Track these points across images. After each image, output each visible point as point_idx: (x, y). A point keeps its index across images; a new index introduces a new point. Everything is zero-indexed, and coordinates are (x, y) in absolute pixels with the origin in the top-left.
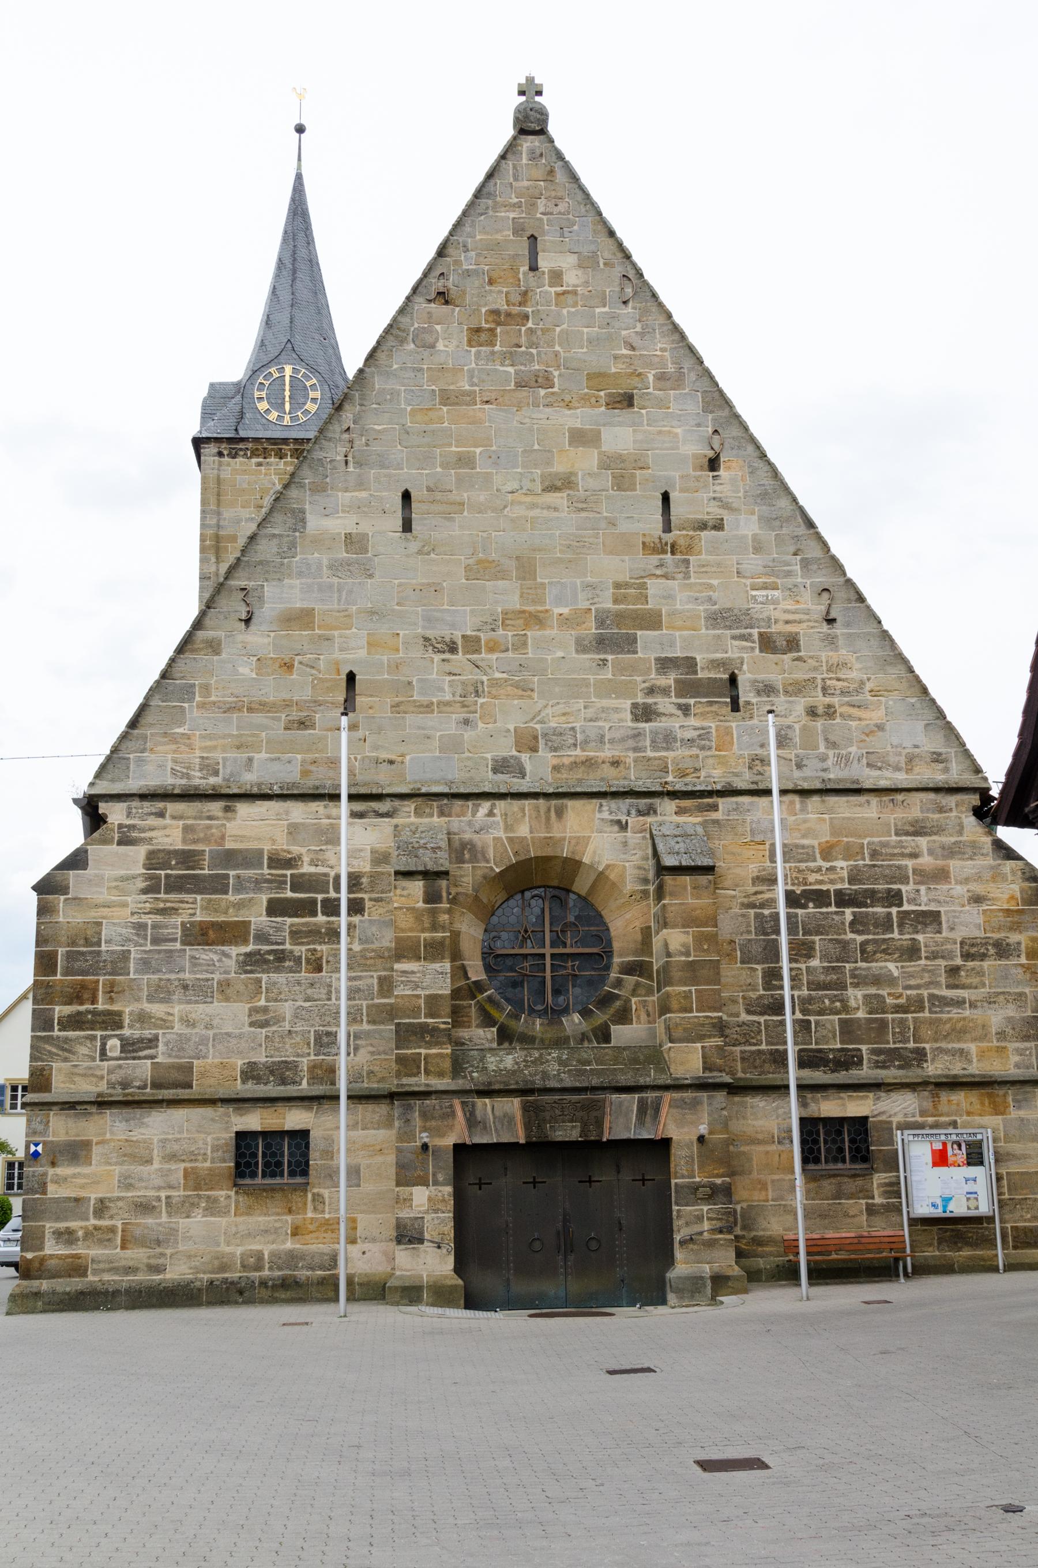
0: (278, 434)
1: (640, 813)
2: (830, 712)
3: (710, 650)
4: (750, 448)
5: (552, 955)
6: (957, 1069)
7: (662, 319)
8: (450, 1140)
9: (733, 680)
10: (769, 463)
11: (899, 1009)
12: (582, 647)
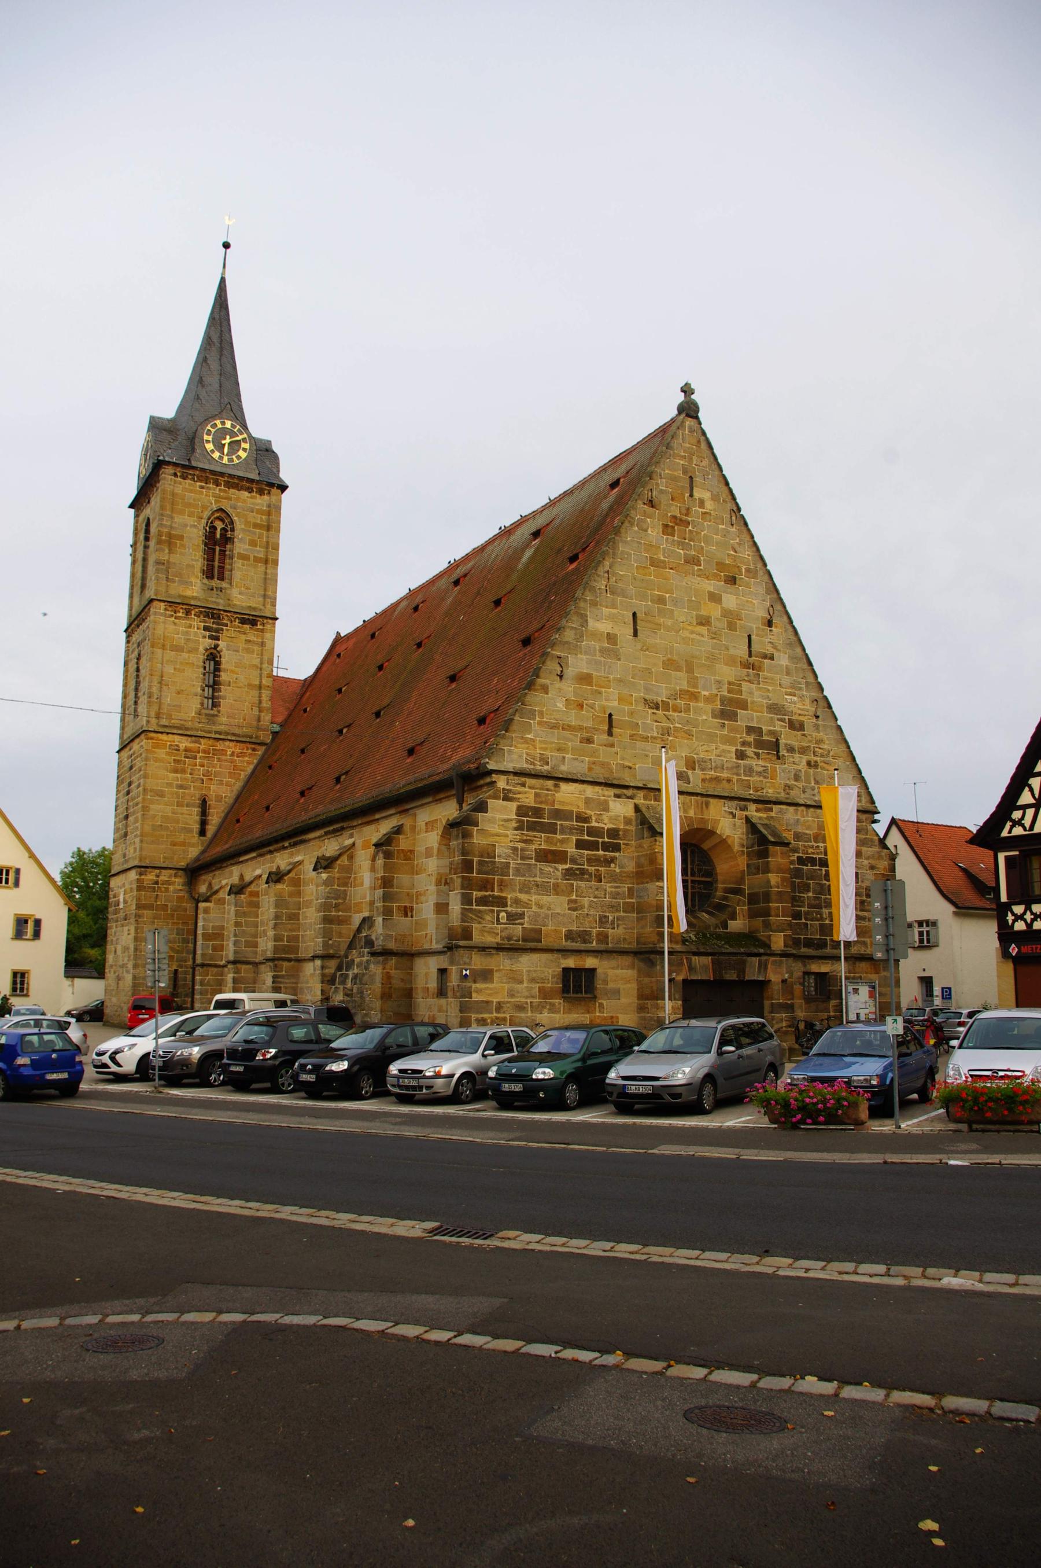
0: (218, 469)
1: (741, 810)
2: (816, 765)
4: (785, 618)
5: (692, 881)
7: (748, 538)
10: (794, 628)
12: (714, 716)
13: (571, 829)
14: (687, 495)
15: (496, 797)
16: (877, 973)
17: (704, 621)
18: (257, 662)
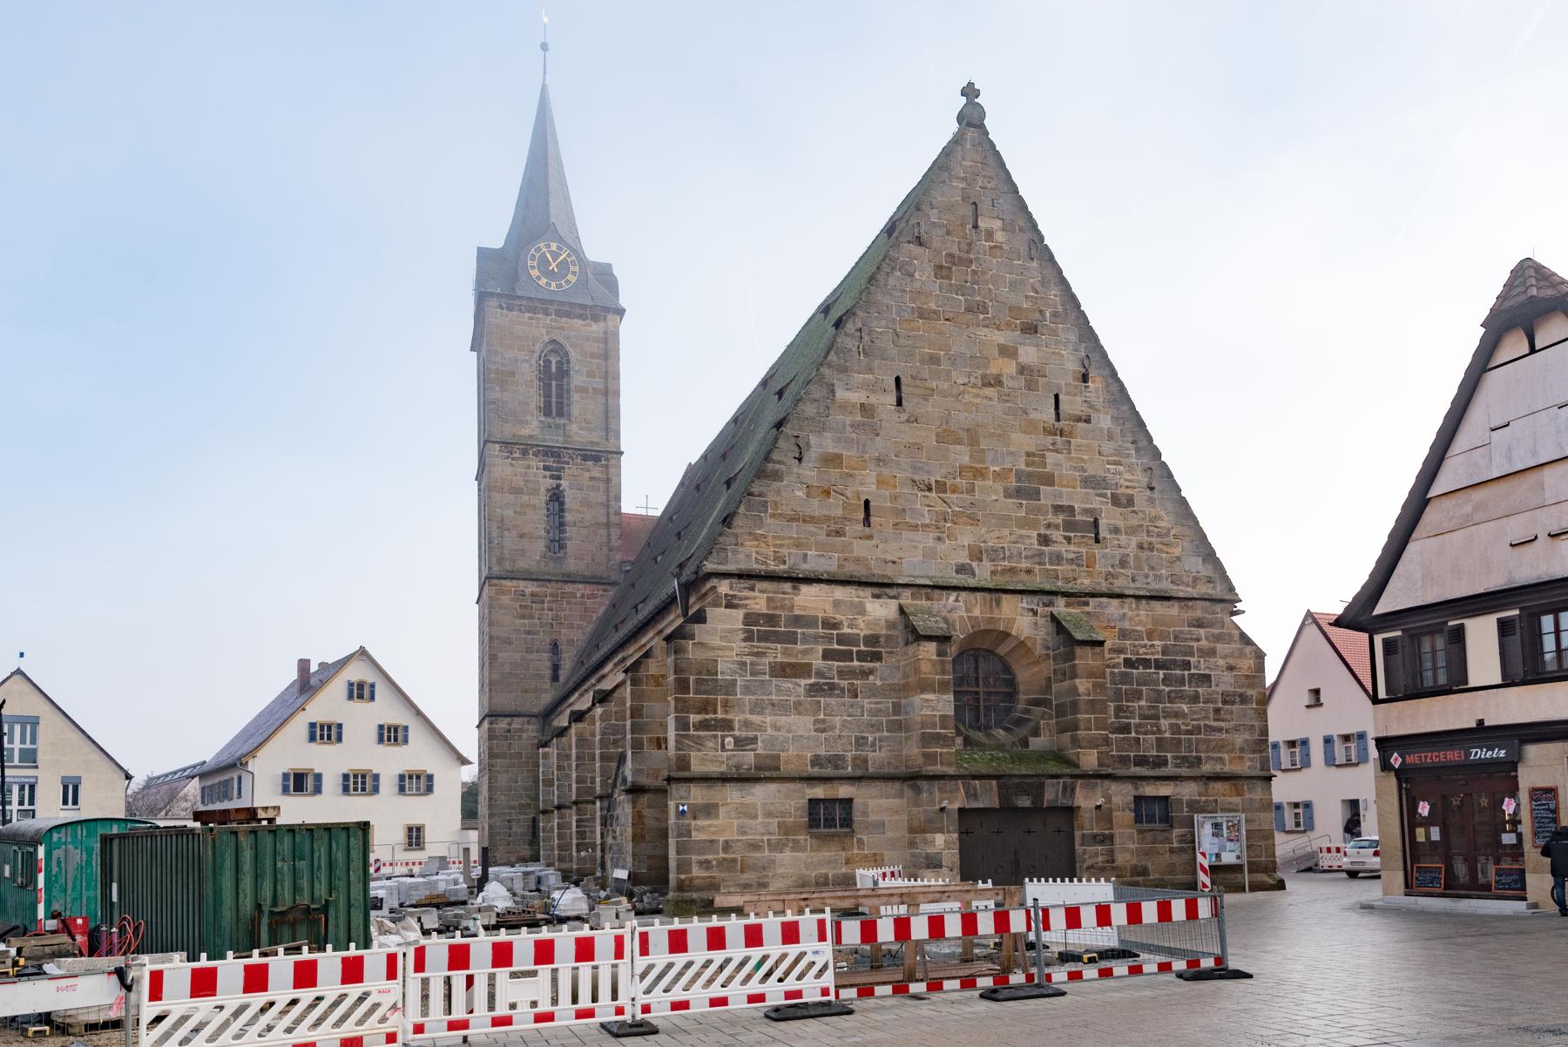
1: (1045, 605)
3: (1081, 500)
6: (1218, 768)
8: (956, 805)
9: (1096, 522)
11: (1188, 732)
12: (1008, 495)
13: (816, 638)
15: (716, 605)
17: (997, 382)
18: (602, 499)
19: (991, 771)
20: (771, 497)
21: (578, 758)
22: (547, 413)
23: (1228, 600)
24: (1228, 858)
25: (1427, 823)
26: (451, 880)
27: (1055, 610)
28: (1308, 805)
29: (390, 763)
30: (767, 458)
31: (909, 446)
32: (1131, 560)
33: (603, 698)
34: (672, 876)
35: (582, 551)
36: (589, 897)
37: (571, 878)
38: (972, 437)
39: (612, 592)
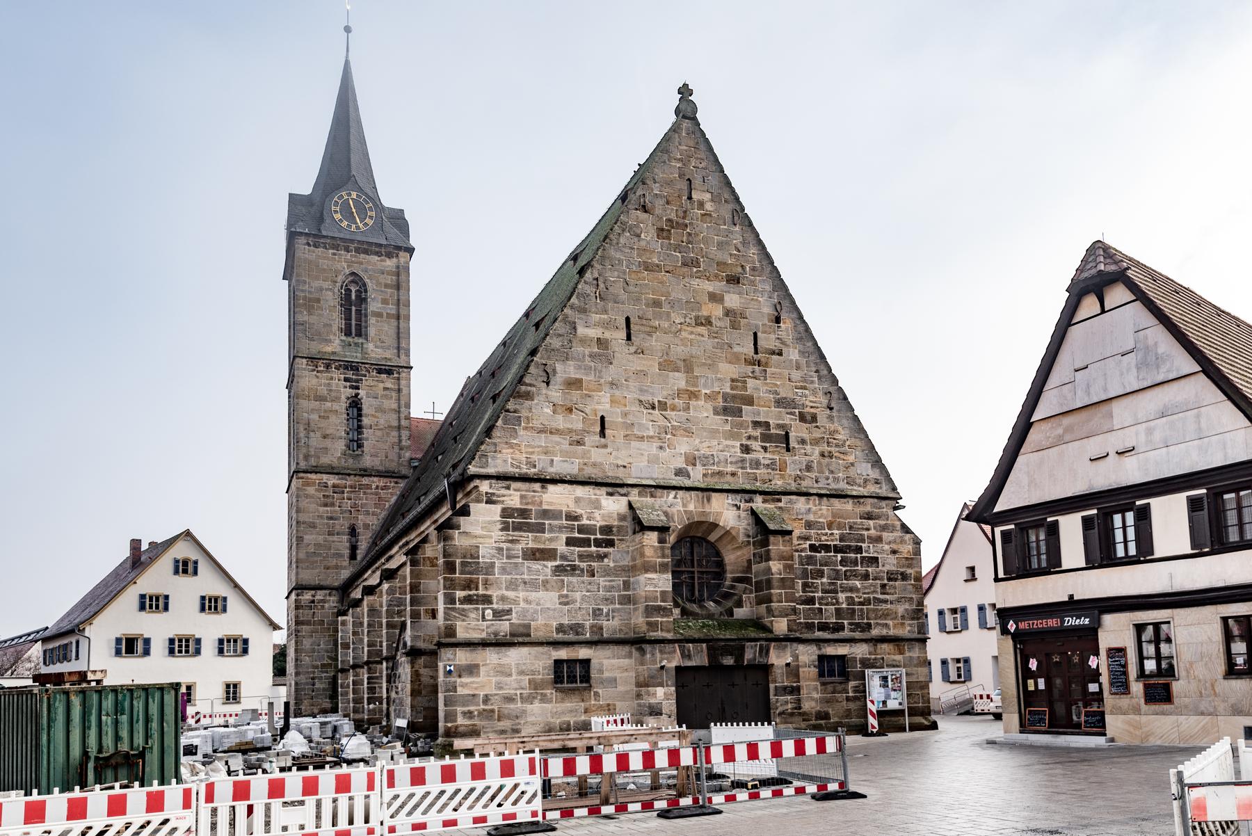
1: (746, 501)
3: (774, 416)
6: (884, 632)
8: (674, 664)
11: (861, 604)
12: (716, 413)
13: (561, 528)
14: (685, 198)
15: (478, 501)
16: (901, 653)
17: (708, 322)
18: (395, 406)
19: (702, 636)
20: (524, 413)
21: (369, 625)
22: (348, 334)
23: (893, 500)
24: (893, 705)
25: (1035, 676)
26: (256, 731)
27: (754, 505)
28: (967, 661)
29: (210, 629)
30: (520, 381)
31: (637, 373)
32: (815, 465)
33: (389, 575)
34: (441, 724)
35: (376, 450)
36: (372, 742)
37: (360, 727)
38: (688, 366)
39: (402, 484)
